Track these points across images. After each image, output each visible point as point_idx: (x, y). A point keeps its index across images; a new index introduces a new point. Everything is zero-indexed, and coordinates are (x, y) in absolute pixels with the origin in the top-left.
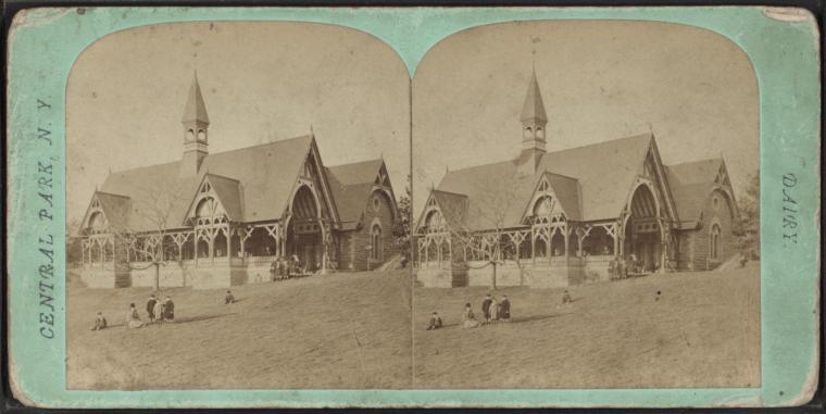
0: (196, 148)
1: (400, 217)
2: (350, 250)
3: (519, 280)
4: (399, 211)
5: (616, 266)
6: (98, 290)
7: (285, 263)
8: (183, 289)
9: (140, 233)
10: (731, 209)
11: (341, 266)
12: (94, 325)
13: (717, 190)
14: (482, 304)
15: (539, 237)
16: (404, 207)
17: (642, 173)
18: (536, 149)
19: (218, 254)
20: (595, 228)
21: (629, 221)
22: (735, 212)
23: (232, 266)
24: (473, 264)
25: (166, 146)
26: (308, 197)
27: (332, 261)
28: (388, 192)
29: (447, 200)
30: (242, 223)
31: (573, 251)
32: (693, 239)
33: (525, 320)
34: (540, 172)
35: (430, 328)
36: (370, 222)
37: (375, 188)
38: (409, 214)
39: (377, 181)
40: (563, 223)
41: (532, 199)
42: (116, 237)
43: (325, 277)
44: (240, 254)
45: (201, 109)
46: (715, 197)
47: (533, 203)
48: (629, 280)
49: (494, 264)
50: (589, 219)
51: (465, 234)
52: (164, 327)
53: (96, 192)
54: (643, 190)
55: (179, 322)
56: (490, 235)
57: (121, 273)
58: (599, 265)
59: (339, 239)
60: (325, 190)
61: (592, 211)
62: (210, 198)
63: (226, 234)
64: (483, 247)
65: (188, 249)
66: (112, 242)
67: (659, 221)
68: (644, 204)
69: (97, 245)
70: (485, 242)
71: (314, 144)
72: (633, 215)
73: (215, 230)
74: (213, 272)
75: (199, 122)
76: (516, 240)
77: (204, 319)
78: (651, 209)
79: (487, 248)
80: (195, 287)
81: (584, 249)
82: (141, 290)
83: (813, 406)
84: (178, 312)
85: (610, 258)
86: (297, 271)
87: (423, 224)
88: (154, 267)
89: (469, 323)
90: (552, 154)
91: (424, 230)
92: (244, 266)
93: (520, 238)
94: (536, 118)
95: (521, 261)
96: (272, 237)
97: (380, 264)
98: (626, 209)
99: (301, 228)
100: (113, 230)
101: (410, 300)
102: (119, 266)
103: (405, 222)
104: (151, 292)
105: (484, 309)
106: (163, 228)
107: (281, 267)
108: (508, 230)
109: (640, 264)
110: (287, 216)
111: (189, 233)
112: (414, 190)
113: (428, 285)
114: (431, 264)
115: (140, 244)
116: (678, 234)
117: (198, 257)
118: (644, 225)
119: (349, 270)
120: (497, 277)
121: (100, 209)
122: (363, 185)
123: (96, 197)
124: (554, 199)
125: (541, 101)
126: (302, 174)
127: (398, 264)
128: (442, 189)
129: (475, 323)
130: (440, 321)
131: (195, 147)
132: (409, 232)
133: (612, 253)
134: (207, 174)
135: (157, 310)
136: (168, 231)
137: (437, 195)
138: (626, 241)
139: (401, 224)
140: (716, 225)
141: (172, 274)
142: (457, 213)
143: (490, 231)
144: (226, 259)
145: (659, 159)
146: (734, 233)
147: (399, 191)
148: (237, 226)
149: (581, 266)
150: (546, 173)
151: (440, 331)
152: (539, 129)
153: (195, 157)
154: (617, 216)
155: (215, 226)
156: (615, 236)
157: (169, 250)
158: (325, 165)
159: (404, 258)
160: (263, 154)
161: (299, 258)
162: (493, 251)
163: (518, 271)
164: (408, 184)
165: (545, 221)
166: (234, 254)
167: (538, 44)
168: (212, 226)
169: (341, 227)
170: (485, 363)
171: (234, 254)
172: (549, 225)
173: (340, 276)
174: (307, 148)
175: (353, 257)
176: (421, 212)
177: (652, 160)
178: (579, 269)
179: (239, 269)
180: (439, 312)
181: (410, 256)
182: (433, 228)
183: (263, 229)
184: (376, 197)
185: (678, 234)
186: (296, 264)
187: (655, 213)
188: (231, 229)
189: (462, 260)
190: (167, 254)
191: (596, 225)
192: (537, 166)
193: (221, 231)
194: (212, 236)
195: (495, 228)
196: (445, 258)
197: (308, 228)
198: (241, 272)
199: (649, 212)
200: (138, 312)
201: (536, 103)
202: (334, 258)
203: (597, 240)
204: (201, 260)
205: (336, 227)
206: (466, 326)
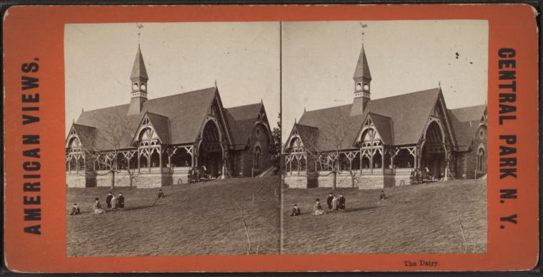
0: (362, 95)
1: (274, 141)
2: (464, 164)
4: (273, 137)
6: (295, 189)
7: (420, 172)
9: (324, 152)
11: (235, 174)
15: (365, 155)
17: (210, 113)
19: (376, 166)
20: (401, 150)
21: (424, 146)
23: (384, 174)
24: (321, 173)
27: (451, 172)
32: (466, 158)
33: (355, 210)
34: (143, 113)
35: (292, 215)
36: (477, 147)
38: (280, 140)
39: (259, 118)
40: (381, 147)
41: (138, 130)
42: (87, 153)
44: (168, 166)
46: (481, 130)
50: (398, 144)
51: (94, 153)
52: (118, 214)
54: (434, 125)
56: (110, 154)
58: (403, 175)
59: (456, 157)
60: (448, 125)
61: (178, 139)
64: (328, 161)
65: (137, 162)
68: (434, 134)
69: (74, 158)
70: (107, 157)
72: (204, 140)
74: (151, 178)
76: (350, 157)
77: (365, 209)
78: (216, 136)
79: (330, 163)
80: (138, 187)
81: (394, 164)
82: (324, 189)
84: (126, 204)
85: (410, 170)
86: (206, 177)
88: (111, 174)
90: (151, 100)
91: (289, 151)
94: (140, 77)
96: (411, 155)
97: (260, 173)
99: (432, 150)
102: (89, 173)
103: (277, 145)
104: (331, 191)
105: (107, 202)
107: (418, 175)
108: (122, 150)
109: (208, 172)
110: (422, 141)
112: (284, 120)
113: (291, 186)
114: (72, 172)
116: (457, 155)
119: (240, 176)
120: (337, 181)
122: (250, 120)
125: (144, 65)
127: (271, 173)
128: (301, 124)
129: (102, 211)
130: (78, 209)
131: (361, 95)
133: (412, 167)
134: (147, 113)
137: (77, 128)
141: (123, 177)
142: (89, 139)
143: (334, 151)
147: (273, 125)
150: (147, 113)
151: (299, 217)
153: (361, 101)
154: (416, 142)
159: (275, 169)
161: (207, 167)
162: (112, 164)
163: (129, 176)
164: (279, 120)
166: (164, 166)
167: (365, 28)
175: (242, 168)
176: (287, 139)
179: (167, 175)
180: (298, 204)
181: (280, 167)
182: (73, 149)
183: (406, 149)
184: (258, 128)
185: (457, 155)
186: (206, 172)
188: (385, 149)
189: (314, 170)
191: (402, 148)
192: (364, 109)
194: (372, 154)
196: (303, 169)
197: (436, 150)
198: (168, 177)
199: (438, 140)
200: (321, 204)
201: (141, 68)
202: (453, 170)
203: (404, 159)
204: (364, 171)
205: (455, 149)
206: (316, 213)
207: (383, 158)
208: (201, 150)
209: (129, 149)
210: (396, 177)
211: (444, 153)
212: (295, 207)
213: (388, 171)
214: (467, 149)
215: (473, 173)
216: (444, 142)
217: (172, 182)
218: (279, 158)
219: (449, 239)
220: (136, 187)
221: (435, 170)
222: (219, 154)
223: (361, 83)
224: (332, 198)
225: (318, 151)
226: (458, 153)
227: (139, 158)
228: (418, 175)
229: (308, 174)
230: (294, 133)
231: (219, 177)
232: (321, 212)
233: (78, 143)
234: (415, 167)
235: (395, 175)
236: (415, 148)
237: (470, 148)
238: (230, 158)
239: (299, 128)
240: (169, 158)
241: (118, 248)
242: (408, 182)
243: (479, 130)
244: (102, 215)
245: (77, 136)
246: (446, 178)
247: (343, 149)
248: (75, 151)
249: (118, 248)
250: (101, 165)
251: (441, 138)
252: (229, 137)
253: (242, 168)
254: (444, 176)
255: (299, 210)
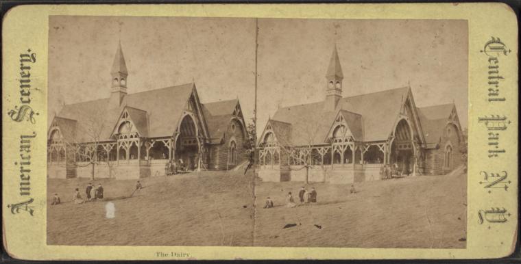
1: (248, 136)
3: (108, 174)
4: (247, 132)
5: (170, 166)
8: (107, 180)
9: (297, 147)
10: (243, 132)
12: (53, 201)
13: (234, 119)
14: (298, 193)
16: (251, 130)
17: (402, 112)
18: (120, 92)
19: (347, 161)
21: (394, 142)
22: (245, 133)
25: (317, 94)
26: (406, 128)
27: (204, 163)
28: (241, 120)
29: (279, 126)
30: (147, 138)
31: (357, 161)
32: (434, 153)
34: (338, 110)
35: (265, 208)
37: (233, 118)
39: (234, 113)
42: (67, 146)
43: (200, 173)
44: (146, 158)
45: (338, 68)
47: (333, 129)
48: (179, 175)
49: (307, 168)
51: (289, 148)
53: (55, 117)
55: (320, 204)
56: (305, 149)
57: (70, 169)
59: (209, 150)
61: (371, 136)
62: (127, 122)
63: (352, 149)
65: (115, 154)
66: (279, 152)
67: (197, 138)
70: (301, 153)
71: (194, 89)
73: (130, 142)
75: (336, 76)
76: (322, 152)
78: (192, 131)
79: (303, 157)
81: (364, 160)
83: (512, 259)
84: (319, 198)
85: (380, 165)
86: (182, 169)
87: (262, 141)
88: (91, 166)
89: (290, 205)
92: (148, 165)
93: (324, 151)
95: (110, 162)
97: (450, 171)
98: (392, 134)
100: (66, 141)
101: (254, 189)
102: (283, 167)
105: (87, 192)
106: (312, 144)
107: (172, 167)
111: (328, 147)
112: (259, 121)
114: (267, 166)
115: (82, 150)
116: (426, 152)
117: (334, 163)
118: (403, 145)
119: (215, 169)
121: (271, 131)
123: (55, 121)
124: (132, 123)
126: (187, 108)
128: (275, 119)
129: (295, 205)
130: (272, 203)
131: (333, 92)
132: (254, 146)
133: (167, 158)
134: (341, 110)
135: (93, 192)
136: (101, 142)
138: (391, 155)
139: (248, 141)
140: (449, 146)
143: (305, 146)
144: (137, 161)
145: (198, 99)
146: (460, 151)
147: (248, 119)
148: (145, 140)
149: (362, 170)
150: (341, 110)
152: (338, 82)
153: (333, 99)
154: (171, 135)
155: (345, 143)
156: (169, 148)
157: (101, 154)
158: (417, 106)
160: (377, 99)
162: (92, 156)
165: (340, 141)
168: (343, 143)
169: (210, 142)
170: (88, 226)
171: (142, 158)
172: (342, 144)
173: (423, 178)
174: (191, 91)
176: (261, 134)
177: (194, 100)
178: (360, 172)
179: (146, 168)
181: (253, 159)
182: (269, 144)
183: (376, 146)
184: (449, 128)
185: (209, 146)
186: (182, 165)
187: (411, 138)
188: (141, 141)
189: (287, 165)
190: (100, 157)
191: (157, 140)
193: (349, 147)
195: (94, 141)
197: (190, 142)
200: (81, 194)
202: (205, 162)
204: (121, 161)
205: (208, 142)
206: (288, 206)
207: (353, 153)
208: (394, 147)
209: (323, 145)
210: (366, 172)
211: (413, 149)
212: (56, 196)
213: (144, 162)
214: (434, 146)
215: (225, 165)
216: (197, 134)
217: (150, 174)
218: (253, 153)
219: (203, 228)
220: (114, 178)
221: (189, 161)
222: (410, 154)
223: (118, 78)
224: (304, 191)
225: (291, 146)
226: (426, 150)
227: (118, 150)
228: (172, 167)
229: (67, 165)
230: (268, 128)
231: (410, 175)
232: (292, 205)
233: (59, 135)
234: (170, 159)
235: (365, 170)
236: (170, 140)
237: (438, 145)
238: (421, 156)
239: (273, 123)
240: (147, 151)
241: (97, 238)
242: (163, 172)
243: (447, 127)
244: (295, 209)
245: (273, 132)
246: (414, 174)
247: (101, 140)
248: (270, 146)
249: (97, 238)
250: (81, 156)
251: (195, 131)
252: (205, 131)
253: (433, 166)
254: (412, 172)
255: (59, 199)
